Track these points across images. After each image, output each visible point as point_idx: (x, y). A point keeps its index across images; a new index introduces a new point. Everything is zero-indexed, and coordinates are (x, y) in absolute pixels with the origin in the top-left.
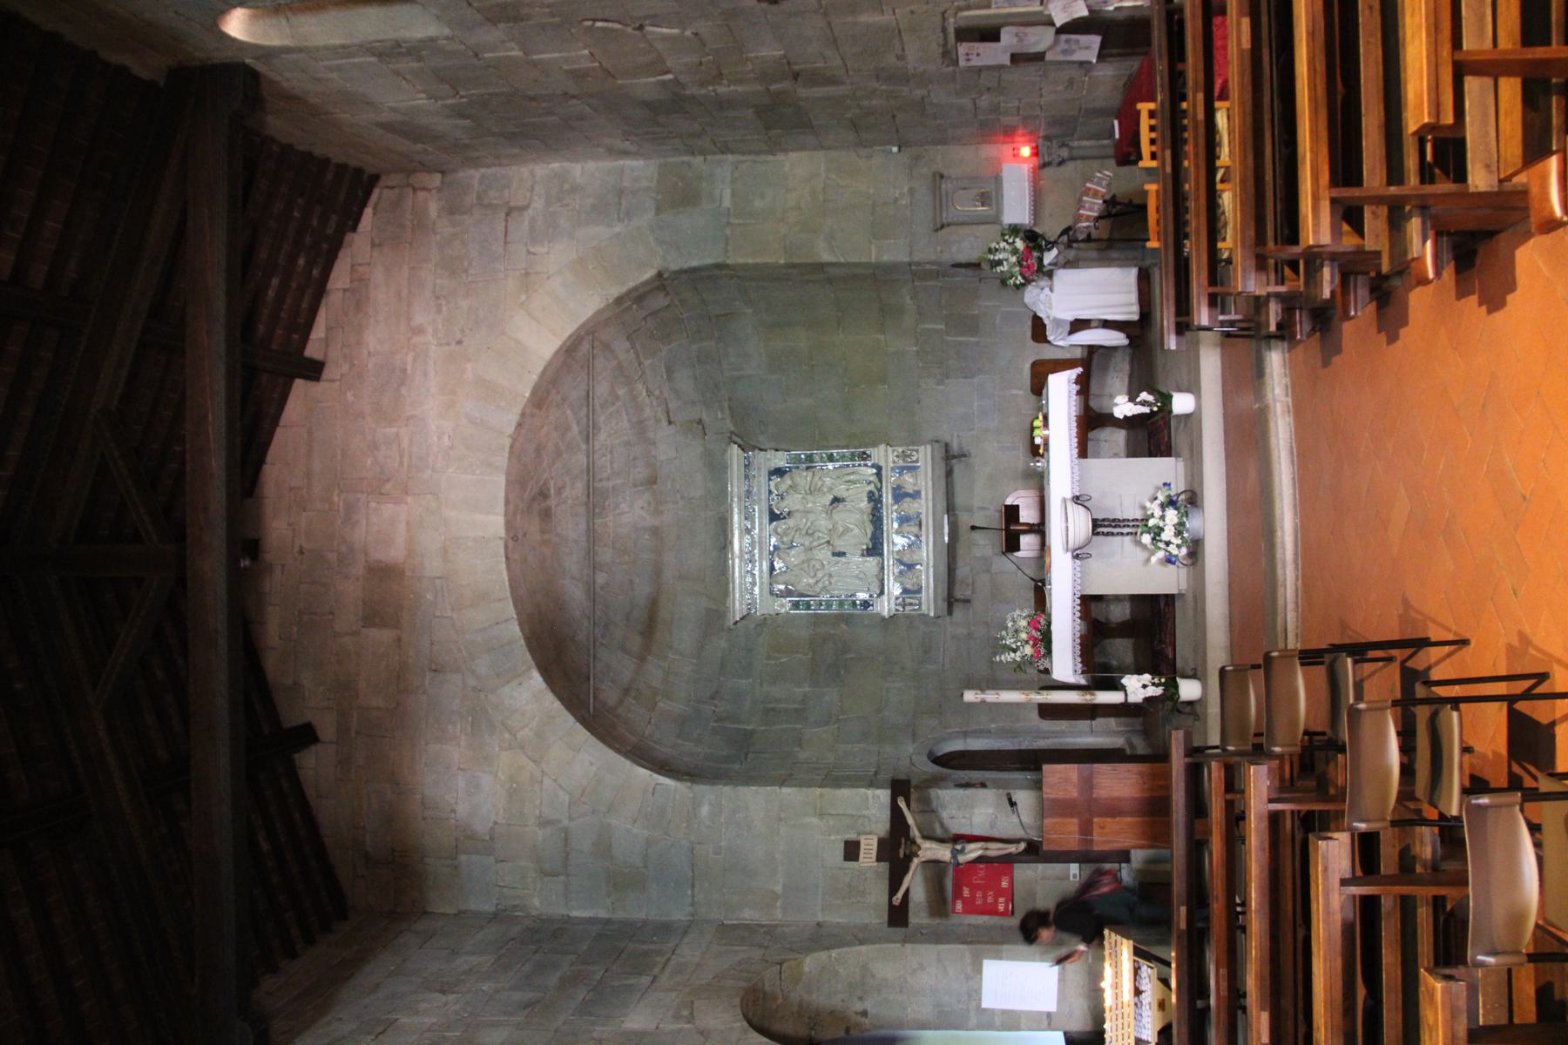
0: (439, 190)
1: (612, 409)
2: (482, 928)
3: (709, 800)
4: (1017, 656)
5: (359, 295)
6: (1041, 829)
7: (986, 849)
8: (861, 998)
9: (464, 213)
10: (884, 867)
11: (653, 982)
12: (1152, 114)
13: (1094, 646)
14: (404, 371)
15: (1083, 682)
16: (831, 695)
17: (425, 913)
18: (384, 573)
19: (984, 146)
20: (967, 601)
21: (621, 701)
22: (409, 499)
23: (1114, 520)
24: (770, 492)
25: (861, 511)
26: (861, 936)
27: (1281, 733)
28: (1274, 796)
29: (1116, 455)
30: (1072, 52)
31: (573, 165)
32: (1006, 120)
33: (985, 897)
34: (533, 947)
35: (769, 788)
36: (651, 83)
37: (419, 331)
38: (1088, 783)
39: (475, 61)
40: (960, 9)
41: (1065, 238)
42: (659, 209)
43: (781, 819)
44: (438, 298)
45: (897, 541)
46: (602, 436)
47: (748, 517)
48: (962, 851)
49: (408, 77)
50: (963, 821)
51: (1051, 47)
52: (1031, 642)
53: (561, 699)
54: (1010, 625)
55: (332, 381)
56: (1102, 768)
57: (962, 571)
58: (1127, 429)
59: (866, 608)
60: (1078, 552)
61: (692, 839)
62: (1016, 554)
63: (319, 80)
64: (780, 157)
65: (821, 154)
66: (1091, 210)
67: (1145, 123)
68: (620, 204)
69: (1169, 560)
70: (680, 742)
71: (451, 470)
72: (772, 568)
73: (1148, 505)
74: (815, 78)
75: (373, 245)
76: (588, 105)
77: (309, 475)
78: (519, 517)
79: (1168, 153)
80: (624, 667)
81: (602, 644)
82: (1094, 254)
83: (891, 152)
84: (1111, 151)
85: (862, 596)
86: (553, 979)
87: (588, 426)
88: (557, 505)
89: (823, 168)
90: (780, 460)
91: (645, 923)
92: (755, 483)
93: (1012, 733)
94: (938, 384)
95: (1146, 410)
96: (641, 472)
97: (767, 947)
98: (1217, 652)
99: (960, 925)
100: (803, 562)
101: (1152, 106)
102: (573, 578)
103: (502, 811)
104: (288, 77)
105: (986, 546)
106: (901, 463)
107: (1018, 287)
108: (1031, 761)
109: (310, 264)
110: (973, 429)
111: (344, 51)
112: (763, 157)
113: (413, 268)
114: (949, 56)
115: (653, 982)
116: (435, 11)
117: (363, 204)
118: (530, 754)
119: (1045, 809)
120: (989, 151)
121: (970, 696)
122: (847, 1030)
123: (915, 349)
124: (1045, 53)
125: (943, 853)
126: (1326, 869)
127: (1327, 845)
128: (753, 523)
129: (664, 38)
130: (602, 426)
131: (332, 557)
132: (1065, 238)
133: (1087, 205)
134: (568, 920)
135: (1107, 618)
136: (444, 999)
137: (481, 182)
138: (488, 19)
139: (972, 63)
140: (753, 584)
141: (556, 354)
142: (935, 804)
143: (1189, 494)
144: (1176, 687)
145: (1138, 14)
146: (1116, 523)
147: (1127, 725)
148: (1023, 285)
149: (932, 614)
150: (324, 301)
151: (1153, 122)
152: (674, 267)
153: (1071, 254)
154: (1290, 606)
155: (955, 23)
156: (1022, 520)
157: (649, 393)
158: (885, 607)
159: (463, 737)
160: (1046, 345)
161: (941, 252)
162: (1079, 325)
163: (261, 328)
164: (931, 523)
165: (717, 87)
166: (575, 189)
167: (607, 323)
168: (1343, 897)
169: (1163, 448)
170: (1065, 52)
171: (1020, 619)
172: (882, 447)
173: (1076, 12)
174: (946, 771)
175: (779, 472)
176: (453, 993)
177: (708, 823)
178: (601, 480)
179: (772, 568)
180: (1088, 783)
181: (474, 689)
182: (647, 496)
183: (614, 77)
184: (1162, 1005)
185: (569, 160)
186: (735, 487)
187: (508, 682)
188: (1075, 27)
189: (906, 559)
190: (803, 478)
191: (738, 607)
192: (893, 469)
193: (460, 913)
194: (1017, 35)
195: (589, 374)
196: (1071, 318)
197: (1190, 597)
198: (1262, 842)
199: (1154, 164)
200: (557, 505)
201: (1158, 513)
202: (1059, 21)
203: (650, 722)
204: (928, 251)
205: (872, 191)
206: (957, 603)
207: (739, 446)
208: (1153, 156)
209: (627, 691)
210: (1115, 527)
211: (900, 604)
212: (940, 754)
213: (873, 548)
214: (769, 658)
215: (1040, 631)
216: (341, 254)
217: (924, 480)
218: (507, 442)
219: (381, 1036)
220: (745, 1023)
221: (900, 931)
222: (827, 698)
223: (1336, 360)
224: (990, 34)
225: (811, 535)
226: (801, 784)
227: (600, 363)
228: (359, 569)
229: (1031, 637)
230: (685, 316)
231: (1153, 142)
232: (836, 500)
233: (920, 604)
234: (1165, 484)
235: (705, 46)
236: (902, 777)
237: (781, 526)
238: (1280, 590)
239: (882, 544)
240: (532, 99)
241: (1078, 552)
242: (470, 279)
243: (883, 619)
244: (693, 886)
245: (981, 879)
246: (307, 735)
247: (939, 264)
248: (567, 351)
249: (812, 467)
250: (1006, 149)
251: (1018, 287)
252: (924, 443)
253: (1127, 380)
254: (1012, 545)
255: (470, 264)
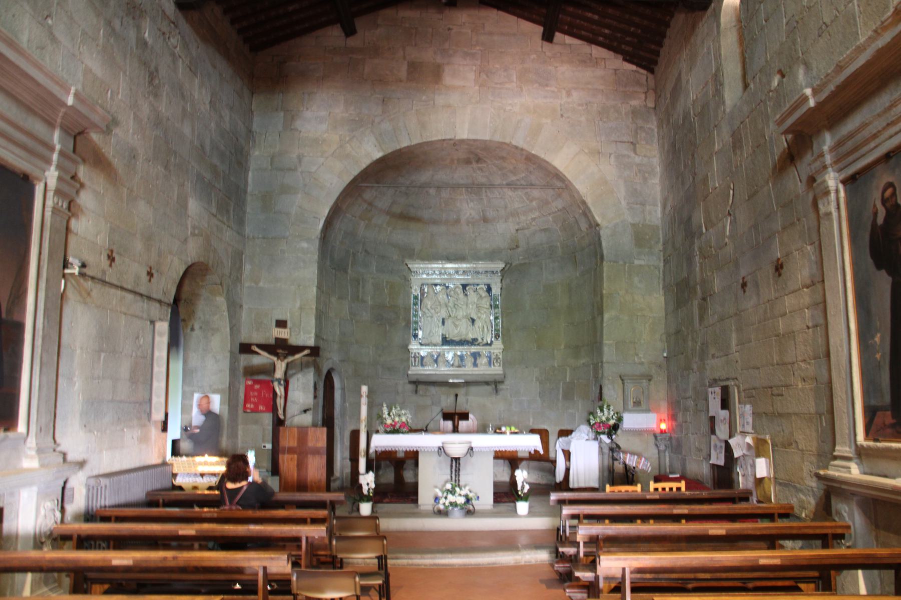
0: (646, 106)
1: (524, 198)
2: (244, 124)
3: (310, 248)
4: (386, 415)
5: (588, 62)
6: (291, 427)
7: (281, 397)
8: (201, 328)
9: (633, 120)
10: (272, 342)
11: (213, 215)
12: (679, 489)
13: (391, 462)
14: (547, 85)
15: (372, 450)
16: (366, 316)
17: (253, 94)
18: (437, 73)
19: (667, 404)
20: (416, 392)
21: (365, 201)
22: (477, 88)
23: (459, 469)
24: (478, 285)
25: (467, 334)
26: (234, 328)
27: (343, 544)
28: (310, 540)
29: (495, 475)
30: (715, 450)
31: (658, 179)
32: (680, 415)
33: (254, 397)
34: (233, 151)
35: (316, 280)
36: (701, 220)
37: (569, 94)
38: (316, 452)
39: (712, 125)
40: (738, 387)
41: (614, 446)
42: (633, 225)
43: (299, 286)
44: (586, 104)
45: (450, 355)
46: (510, 193)
47: (464, 272)
48: (280, 384)
49: (705, 90)
50: (296, 386)
51: (718, 438)
52: (393, 423)
53: (366, 169)
54: (403, 412)
55: (542, 47)
56: (323, 460)
57: (433, 390)
58: (510, 482)
59: (414, 336)
60: (442, 450)
61: (290, 238)
62: (442, 419)
63: (703, 42)
64: (662, 292)
65: (663, 314)
66: (630, 460)
67: (674, 485)
68: (637, 204)
69: (437, 499)
70: (342, 232)
71: (492, 110)
72: (436, 285)
73: (467, 488)
74: (703, 310)
75: (615, 70)
76: (690, 186)
77: (491, 34)
78: (466, 147)
79: (657, 497)
80: (384, 202)
81: (396, 191)
82: (606, 463)
83: (664, 351)
84: (662, 472)
85: (420, 334)
86: (216, 161)
87: (516, 185)
88: (472, 168)
89: (655, 315)
90: (496, 290)
91: (244, 212)
92: (483, 276)
93: (343, 415)
94: (536, 378)
95: (519, 488)
96: (490, 214)
97: (230, 277)
98: (387, 524)
99: (239, 383)
100: (440, 302)
101: (683, 489)
102: (433, 176)
103: (307, 135)
104: (703, 27)
105: (447, 402)
106: (493, 357)
107: (588, 421)
108: (328, 422)
109: (605, 36)
110: (511, 397)
111: (718, 56)
112: (661, 282)
113: (603, 92)
114: (714, 382)
115: (213, 215)
116: (738, 104)
117: (638, 65)
118: (337, 151)
119: (303, 432)
120: (664, 406)
121: (364, 389)
122: (184, 320)
123: (556, 365)
124: (715, 435)
125: (279, 374)
126: (272, 559)
127: (284, 560)
128: (461, 275)
129: (724, 227)
130: (516, 193)
131: (447, 46)
132: (614, 446)
133: (632, 458)
134: (247, 171)
135: (405, 469)
136: (207, 102)
137: (650, 128)
138: (734, 132)
139: (710, 395)
140: (428, 274)
141: (555, 168)
142: (306, 370)
143: (473, 511)
144: (368, 501)
145: (735, 484)
146: (458, 471)
147: (346, 478)
148: (590, 423)
149: (410, 372)
150: (586, 43)
151: (674, 489)
152: (602, 233)
153: (606, 450)
154: (410, 561)
155: (732, 385)
156: (460, 422)
157: (534, 219)
158: (414, 347)
159: (347, 115)
160: (557, 437)
161: (608, 379)
162: (567, 454)
163: (571, 9)
164: (460, 373)
165: (698, 256)
166: (645, 179)
167: (572, 196)
168: (257, 568)
169: (499, 499)
170: (716, 446)
171: (406, 416)
172: (502, 347)
173: (736, 451)
174: (323, 378)
175: (489, 290)
176: (210, 108)
177: (298, 246)
178: (486, 192)
179: (436, 285)
180: (316, 452)
181: (373, 121)
182: (477, 217)
183: (704, 200)
184: (195, 488)
185: (661, 176)
186: (482, 265)
187: (377, 139)
188: (728, 449)
189: (440, 359)
190: (486, 303)
191: (415, 266)
192: (490, 352)
193: (252, 112)
194: (724, 419)
195: (544, 186)
196: (571, 451)
197: (415, 510)
198: (285, 532)
199: (652, 489)
200: (472, 168)
201: (463, 492)
202: (731, 441)
203: (353, 216)
204: (609, 371)
205: (642, 341)
206: (415, 386)
207: (504, 268)
208: (656, 489)
209: (370, 204)
210: (456, 471)
211: (415, 355)
212: (333, 374)
213: (446, 341)
214: (387, 282)
215: (399, 428)
216: (611, 53)
217: (484, 369)
218: (507, 141)
219: (188, 69)
220: (190, 264)
221: (237, 350)
222: (364, 314)
223: (544, 586)
224: (725, 404)
225: (454, 306)
226: (318, 299)
227: (551, 192)
228: (439, 60)
229: (396, 423)
230: (575, 239)
231: (664, 489)
232: (473, 321)
233: (415, 366)
234: (478, 497)
235: (720, 249)
236: (321, 353)
237: (460, 290)
238: (419, 556)
239: (449, 345)
240: (693, 156)
241: (442, 450)
242: (597, 122)
243: (407, 345)
244: (264, 238)
245: (264, 395)
246: (350, 32)
247: (602, 377)
248: (557, 174)
249: (491, 308)
250: (665, 416)
251: (588, 421)
252: (504, 370)
253: (537, 482)
254: (447, 416)
255: (604, 122)
